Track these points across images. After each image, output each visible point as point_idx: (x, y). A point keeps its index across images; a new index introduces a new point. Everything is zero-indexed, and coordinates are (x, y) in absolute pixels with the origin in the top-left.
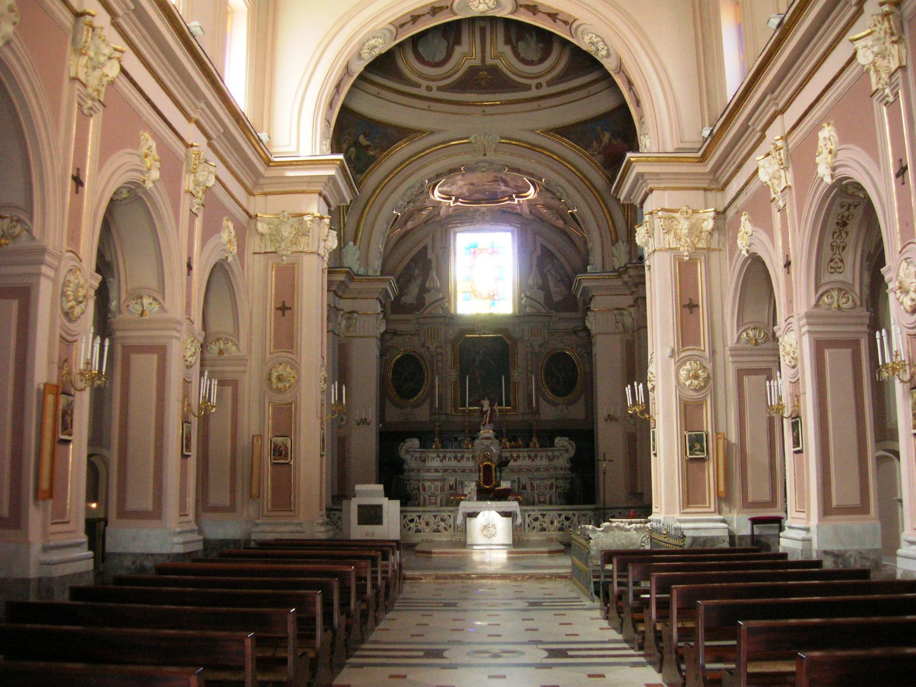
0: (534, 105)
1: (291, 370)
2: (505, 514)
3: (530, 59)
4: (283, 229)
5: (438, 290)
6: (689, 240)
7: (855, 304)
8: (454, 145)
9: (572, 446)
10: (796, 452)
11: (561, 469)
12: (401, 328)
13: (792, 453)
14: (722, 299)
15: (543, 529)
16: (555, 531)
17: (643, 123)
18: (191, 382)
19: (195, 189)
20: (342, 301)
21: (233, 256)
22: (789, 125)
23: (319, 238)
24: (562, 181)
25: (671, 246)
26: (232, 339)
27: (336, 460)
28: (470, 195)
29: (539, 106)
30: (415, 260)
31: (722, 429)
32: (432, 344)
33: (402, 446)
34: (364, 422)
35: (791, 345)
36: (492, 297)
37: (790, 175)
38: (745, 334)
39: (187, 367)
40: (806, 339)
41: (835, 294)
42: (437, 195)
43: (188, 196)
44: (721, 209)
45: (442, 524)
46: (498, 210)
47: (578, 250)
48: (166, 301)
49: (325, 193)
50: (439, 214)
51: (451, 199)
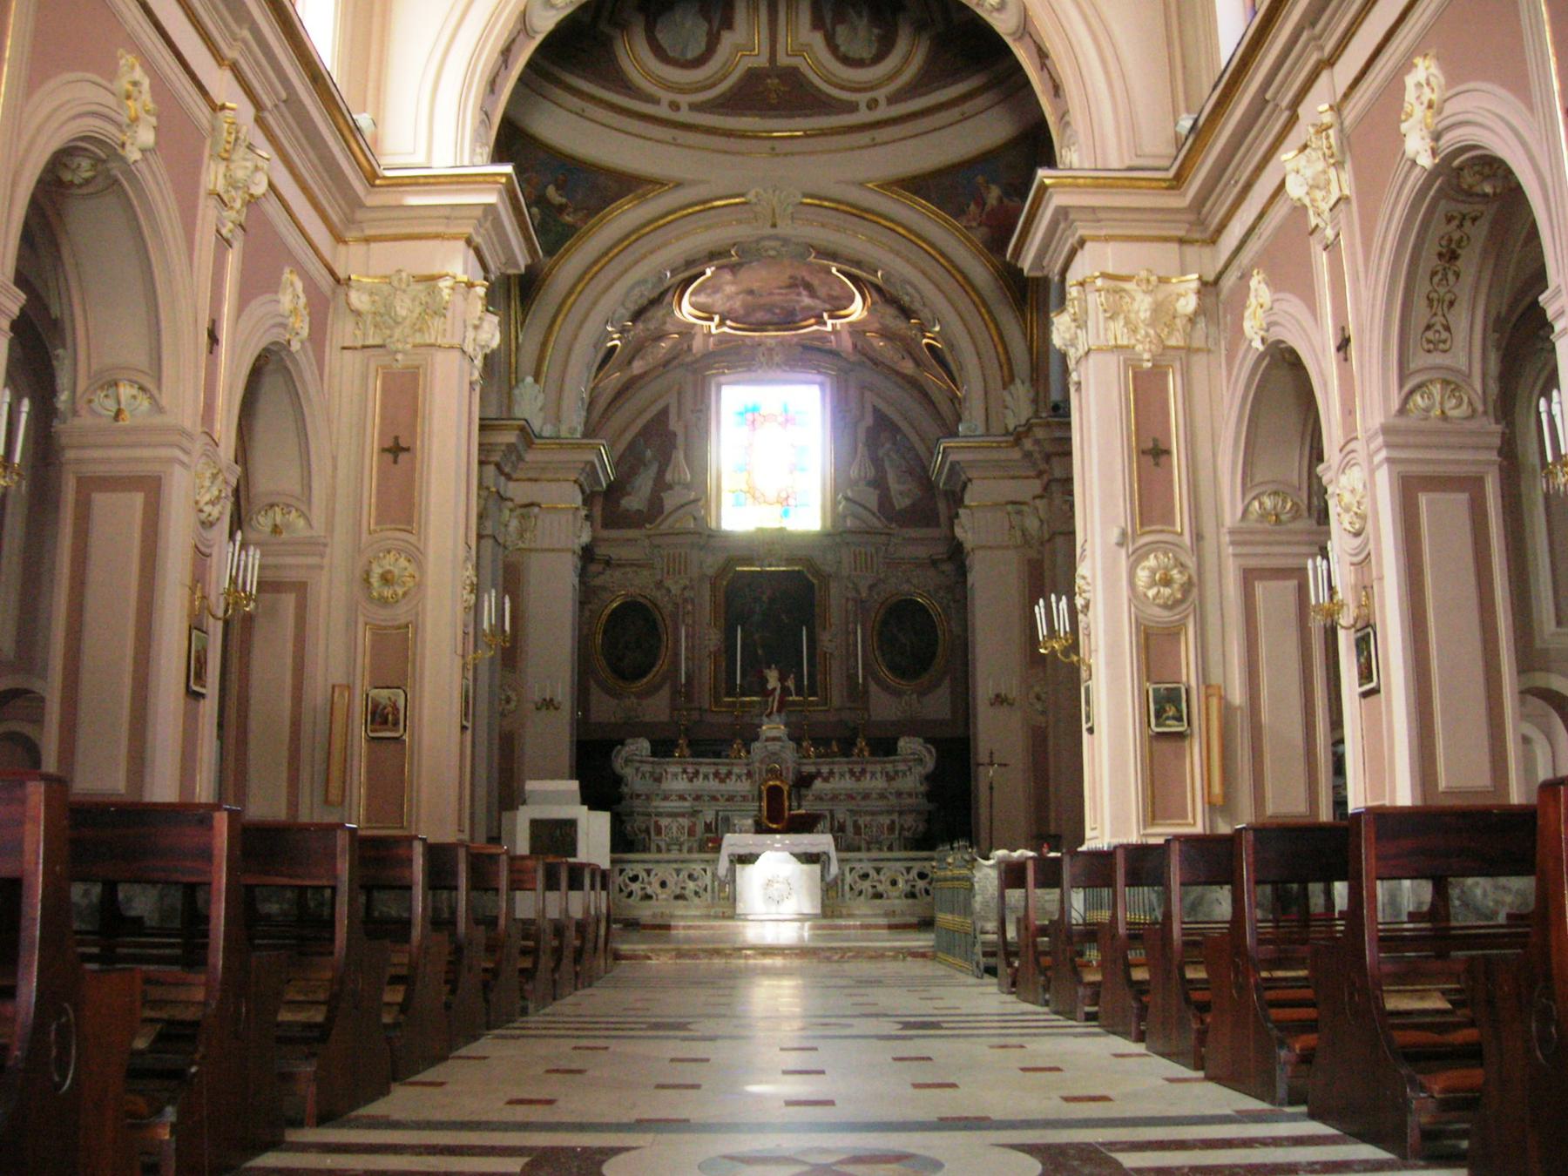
0: (864, 138)
1: (407, 564)
2: (808, 858)
3: (857, 56)
4: (398, 304)
5: (687, 486)
6: (1152, 332)
7: (1474, 411)
8: (718, 207)
9: (930, 752)
10: (1365, 695)
11: (910, 795)
12: (615, 553)
13: (1357, 697)
14: (1213, 441)
15: (878, 896)
16: (899, 897)
17: (1068, 124)
18: (209, 556)
19: (227, 192)
20: (511, 484)
21: (302, 343)
22: (1342, 87)
23: (465, 321)
24: (916, 277)
25: (1119, 342)
26: (294, 502)
27: (495, 765)
28: (747, 314)
29: (874, 139)
30: (646, 432)
31: (1215, 677)
32: (676, 582)
33: (619, 752)
34: (549, 704)
35: (1353, 491)
36: (784, 501)
37: (1346, 176)
38: (1256, 504)
39: (203, 523)
40: (1383, 477)
41: (1436, 390)
42: (686, 311)
43: (213, 202)
44: (1210, 277)
45: (691, 885)
46: (798, 344)
47: (939, 413)
48: (164, 389)
49: (478, 240)
50: (690, 348)
51: (711, 319)
